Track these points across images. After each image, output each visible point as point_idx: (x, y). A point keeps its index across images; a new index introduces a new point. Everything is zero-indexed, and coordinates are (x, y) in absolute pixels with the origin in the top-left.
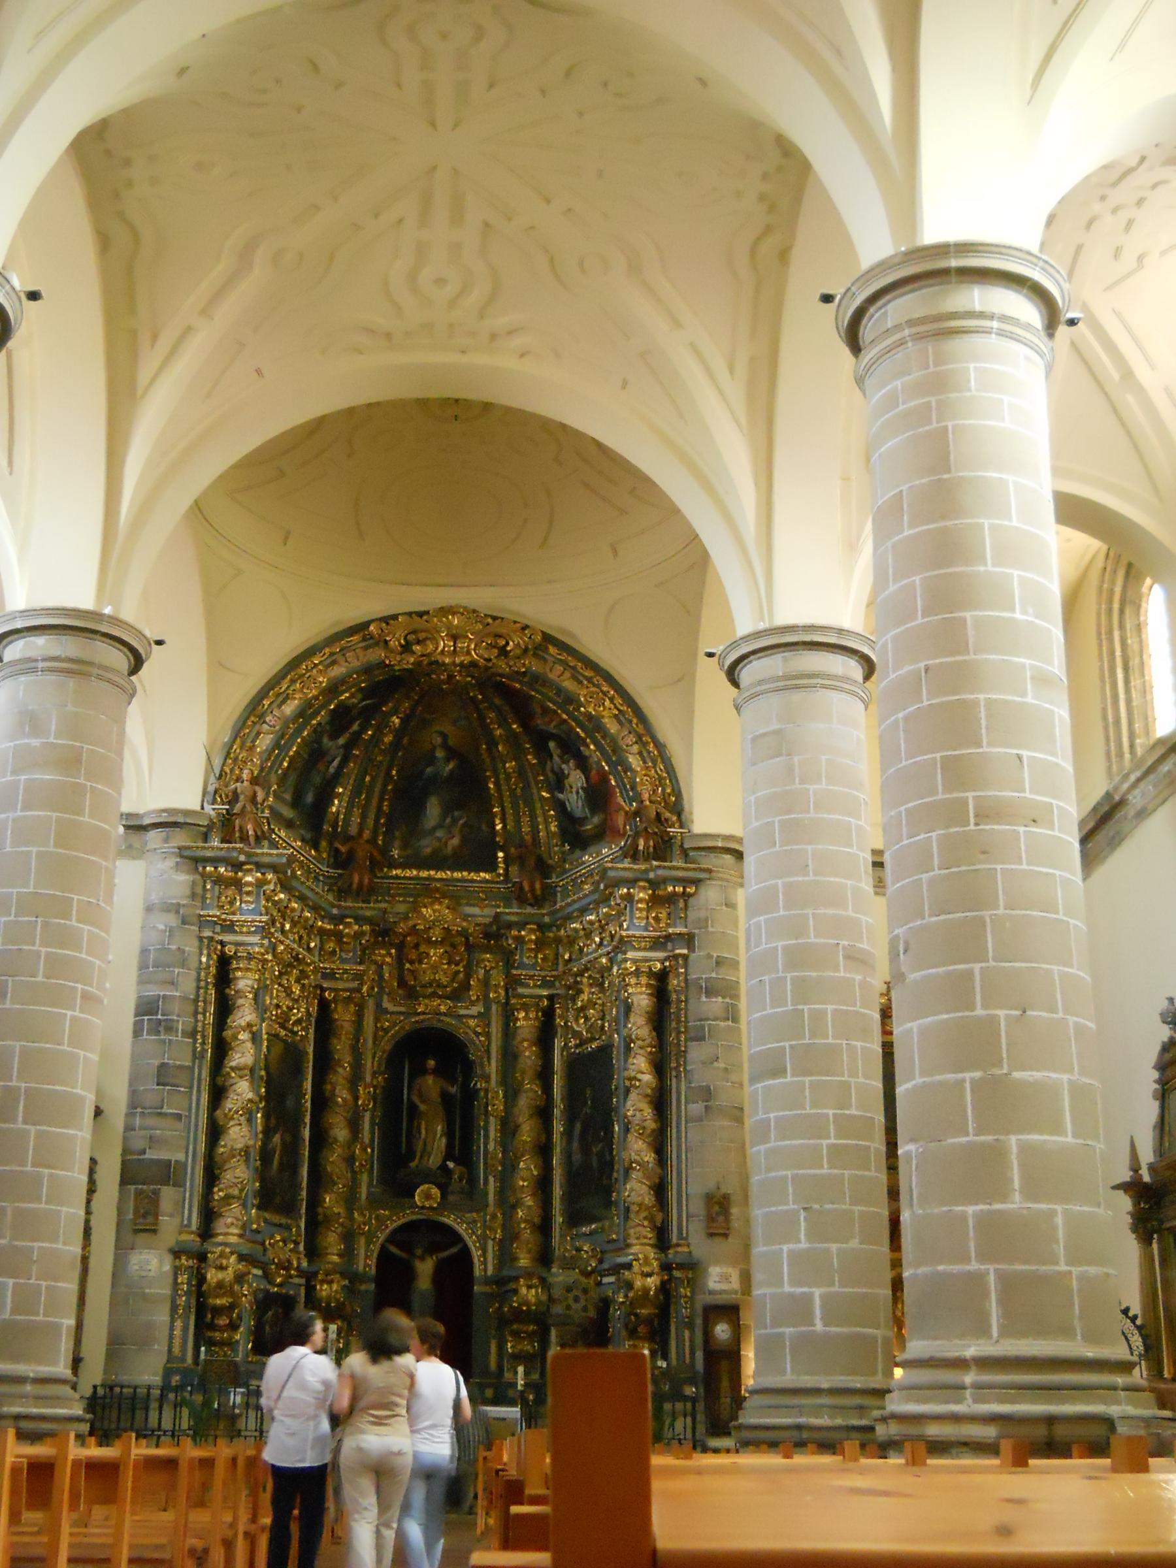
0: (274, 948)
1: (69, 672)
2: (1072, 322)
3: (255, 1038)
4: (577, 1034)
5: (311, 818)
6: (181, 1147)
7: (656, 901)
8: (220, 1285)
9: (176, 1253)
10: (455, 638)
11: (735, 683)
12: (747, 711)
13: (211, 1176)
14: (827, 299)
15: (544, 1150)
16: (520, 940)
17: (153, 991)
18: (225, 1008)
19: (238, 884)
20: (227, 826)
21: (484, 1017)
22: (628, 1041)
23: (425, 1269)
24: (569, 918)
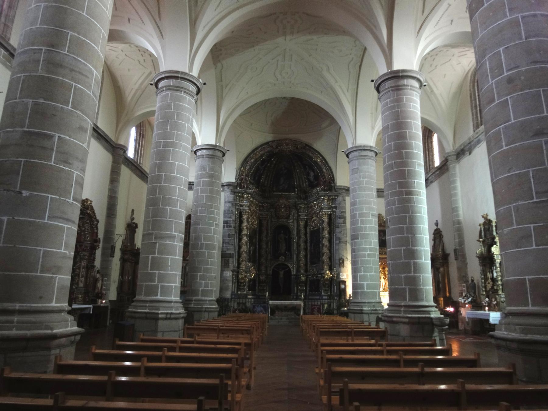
0: (250, 209)
1: (211, 158)
2: (425, 86)
3: (247, 228)
4: (312, 226)
5: (257, 183)
6: (232, 250)
7: (329, 200)
8: (242, 278)
9: (233, 271)
10: (287, 145)
11: (348, 157)
12: (350, 164)
13: (239, 255)
14: (372, 81)
15: (306, 249)
16: (301, 207)
17: (227, 219)
18: (241, 222)
19: (243, 197)
20: (240, 185)
21: (293, 222)
22: (323, 228)
23: (282, 273)
24: (311, 202)
